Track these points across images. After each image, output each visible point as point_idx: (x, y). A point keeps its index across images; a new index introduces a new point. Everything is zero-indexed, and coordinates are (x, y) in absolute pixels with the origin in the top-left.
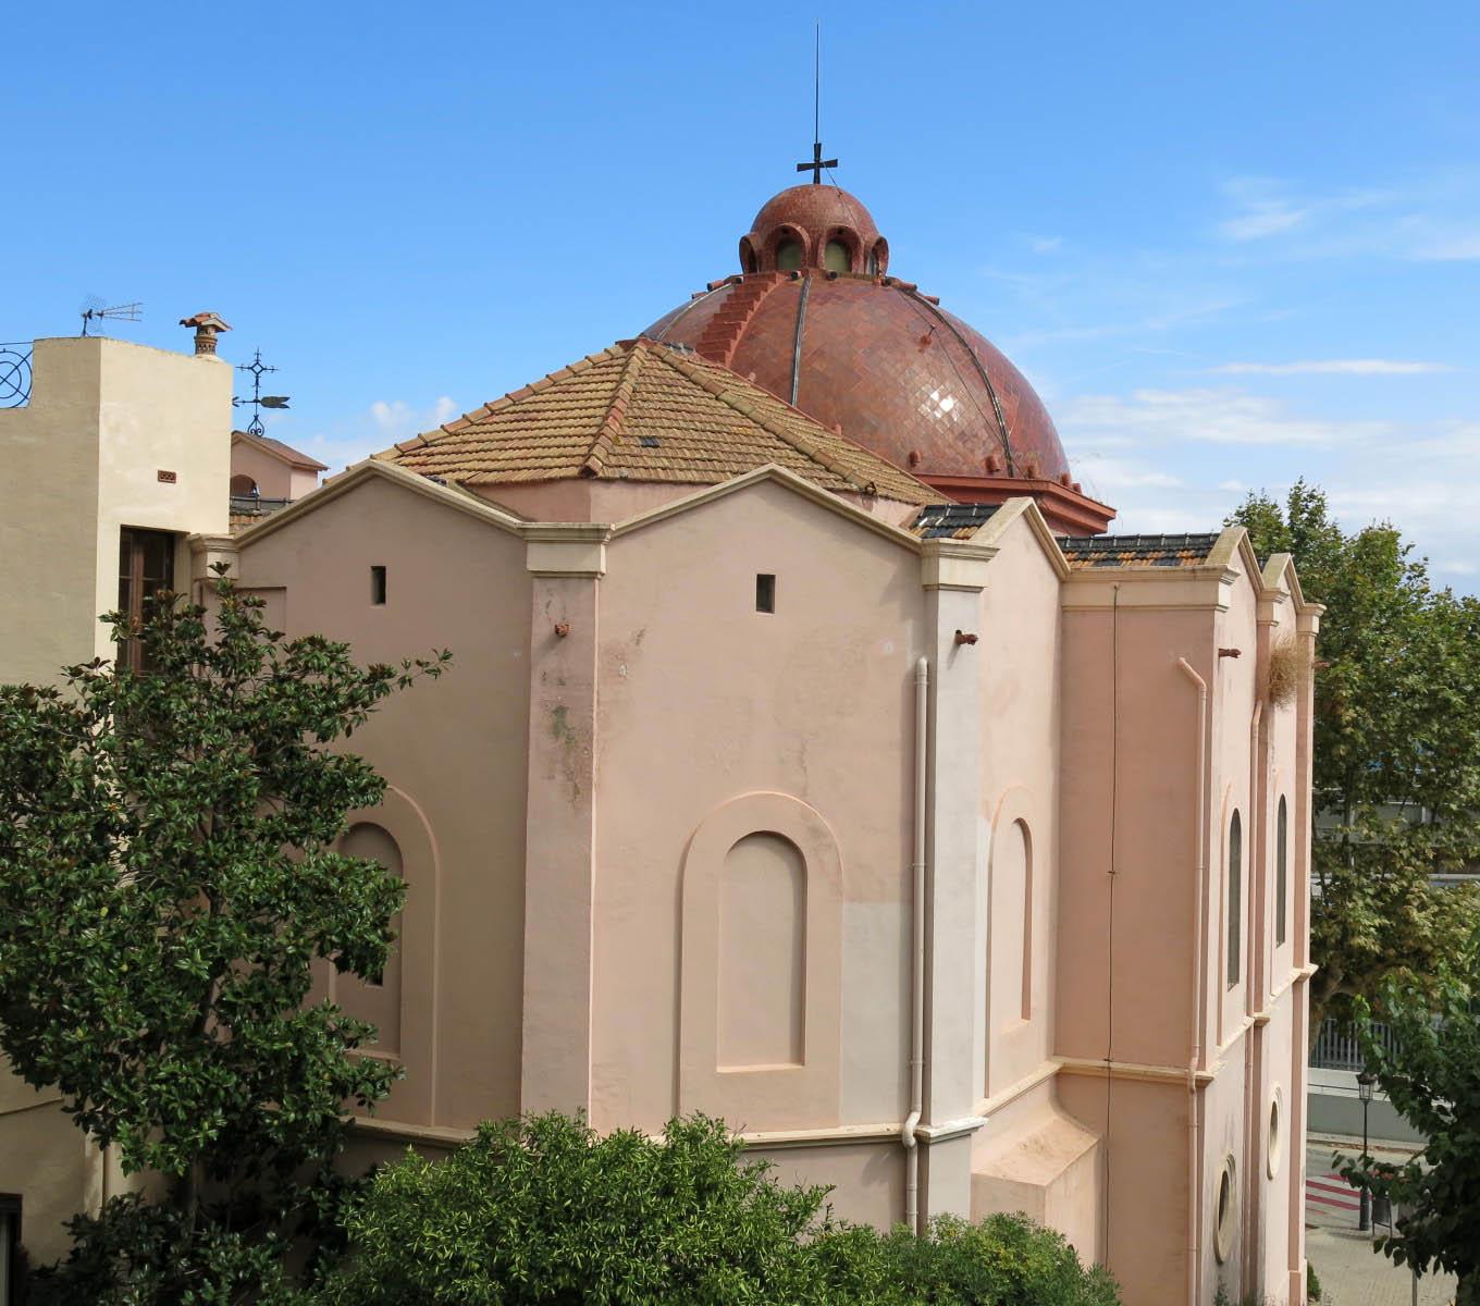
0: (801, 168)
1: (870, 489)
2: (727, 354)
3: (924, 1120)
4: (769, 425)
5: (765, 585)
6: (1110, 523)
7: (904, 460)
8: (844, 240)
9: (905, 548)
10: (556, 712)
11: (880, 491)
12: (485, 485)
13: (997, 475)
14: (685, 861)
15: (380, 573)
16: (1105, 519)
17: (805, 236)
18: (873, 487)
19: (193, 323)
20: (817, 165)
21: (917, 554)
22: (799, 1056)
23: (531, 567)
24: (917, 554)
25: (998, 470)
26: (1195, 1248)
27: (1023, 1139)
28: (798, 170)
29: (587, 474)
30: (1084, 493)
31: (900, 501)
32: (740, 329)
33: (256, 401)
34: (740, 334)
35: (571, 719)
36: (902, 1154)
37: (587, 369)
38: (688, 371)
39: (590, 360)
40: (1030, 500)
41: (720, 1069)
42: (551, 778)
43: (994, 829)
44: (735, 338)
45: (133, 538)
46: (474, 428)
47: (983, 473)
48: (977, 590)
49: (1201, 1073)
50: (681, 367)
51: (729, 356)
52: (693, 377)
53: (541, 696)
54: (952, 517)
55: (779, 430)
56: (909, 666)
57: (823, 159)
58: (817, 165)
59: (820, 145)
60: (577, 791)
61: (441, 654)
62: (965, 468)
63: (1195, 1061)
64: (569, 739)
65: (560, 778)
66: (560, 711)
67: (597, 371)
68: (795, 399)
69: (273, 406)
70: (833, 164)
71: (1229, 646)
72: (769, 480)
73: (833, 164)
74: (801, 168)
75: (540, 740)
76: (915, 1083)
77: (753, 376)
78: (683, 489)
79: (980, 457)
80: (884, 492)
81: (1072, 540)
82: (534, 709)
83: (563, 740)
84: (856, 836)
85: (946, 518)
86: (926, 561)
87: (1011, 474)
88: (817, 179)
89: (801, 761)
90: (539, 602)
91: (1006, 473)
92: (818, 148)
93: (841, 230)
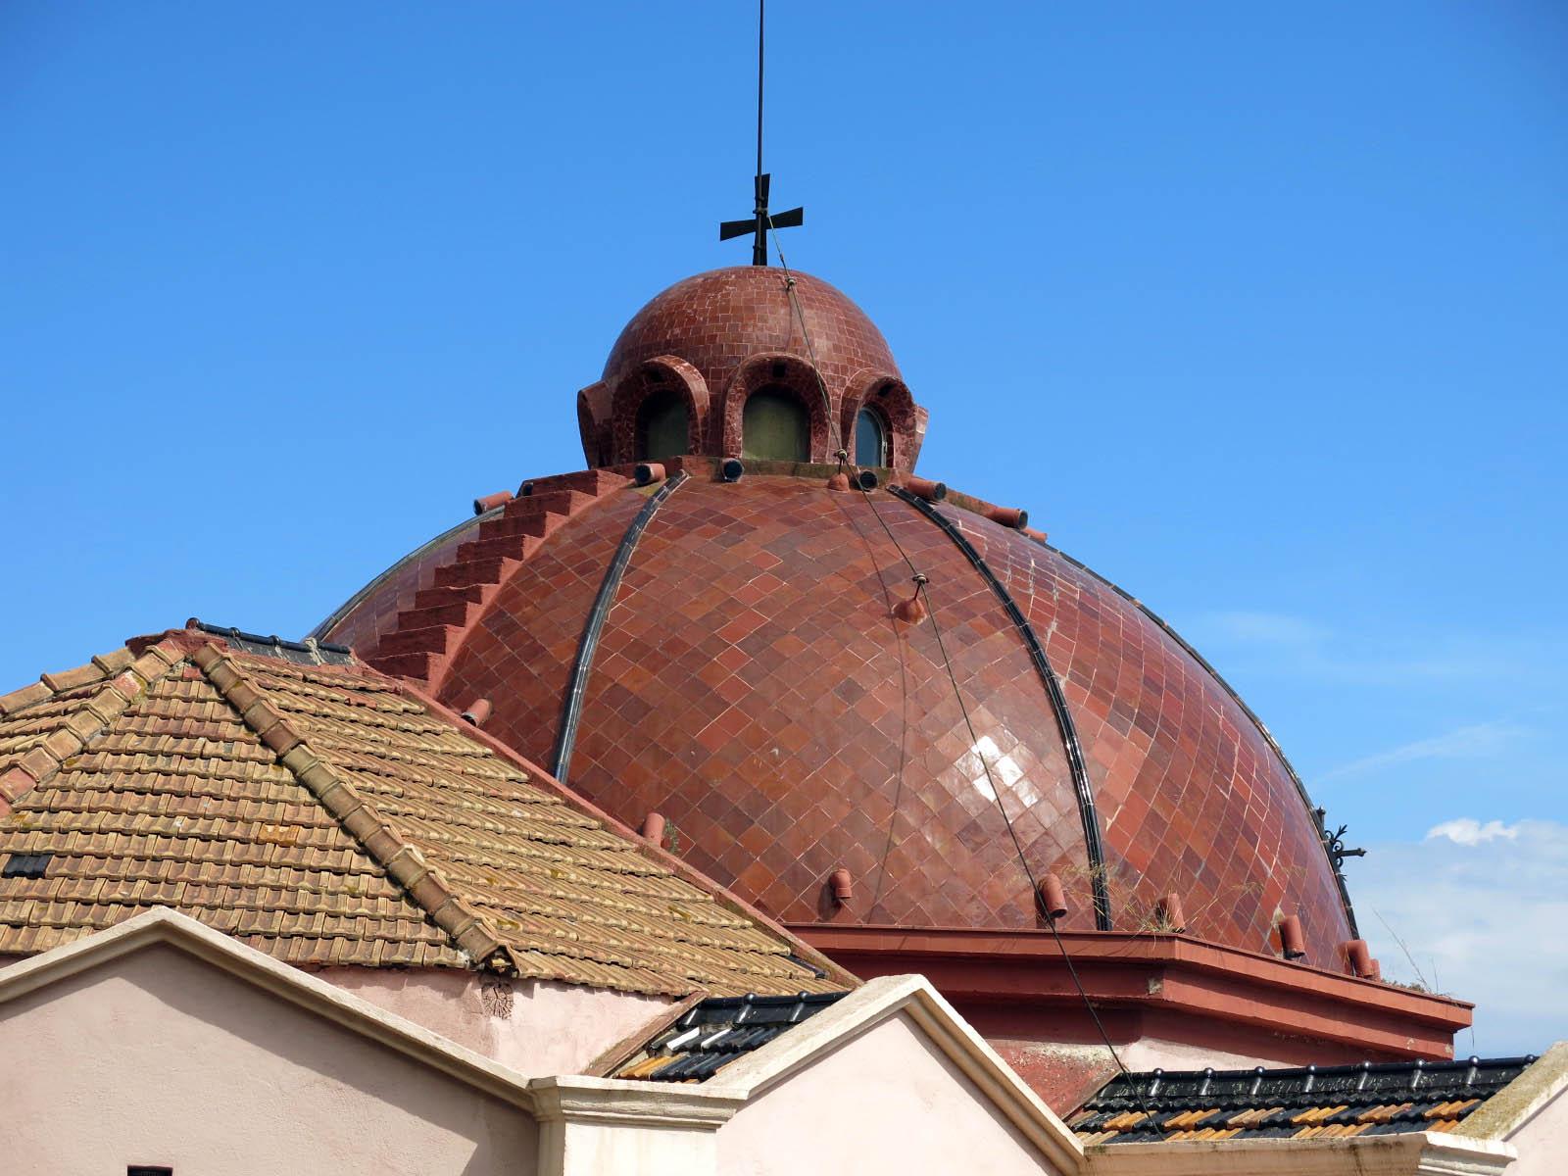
0: (730, 230)
1: (499, 962)
2: (434, 658)
4: (356, 820)
6: (1458, 1036)
7: (807, 896)
8: (786, 388)
9: (492, 1099)
11: (530, 964)
13: (1061, 925)
16: (1446, 1030)
17: (698, 386)
18: (508, 958)
20: (760, 225)
25: (1062, 913)
28: (723, 238)
30: (1387, 976)
31: (612, 989)
32: (479, 601)
34: (475, 613)
37: (36, 703)
38: (246, 700)
39: (48, 684)
40: (917, 982)
44: (461, 622)
47: (1027, 918)
50: (236, 693)
51: (440, 665)
52: (251, 714)
54: (748, 1025)
55: (367, 830)
57: (773, 210)
58: (760, 225)
59: (766, 178)
62: (973, 909)
67: (60, 706)
68: (565, 757)
70: (793, 218)
72: (161, 945)
73: (793, 218)
74: (730, 230)
77: (480, 709)
79: (1017, 883)
81: (1318, 1074)
85: (737, 1027)
86: (545, 1130)
87: (1103, 923)
88: (760, 256)
91: (1092, 920)
92: (763, 184)
93: (779, 367)
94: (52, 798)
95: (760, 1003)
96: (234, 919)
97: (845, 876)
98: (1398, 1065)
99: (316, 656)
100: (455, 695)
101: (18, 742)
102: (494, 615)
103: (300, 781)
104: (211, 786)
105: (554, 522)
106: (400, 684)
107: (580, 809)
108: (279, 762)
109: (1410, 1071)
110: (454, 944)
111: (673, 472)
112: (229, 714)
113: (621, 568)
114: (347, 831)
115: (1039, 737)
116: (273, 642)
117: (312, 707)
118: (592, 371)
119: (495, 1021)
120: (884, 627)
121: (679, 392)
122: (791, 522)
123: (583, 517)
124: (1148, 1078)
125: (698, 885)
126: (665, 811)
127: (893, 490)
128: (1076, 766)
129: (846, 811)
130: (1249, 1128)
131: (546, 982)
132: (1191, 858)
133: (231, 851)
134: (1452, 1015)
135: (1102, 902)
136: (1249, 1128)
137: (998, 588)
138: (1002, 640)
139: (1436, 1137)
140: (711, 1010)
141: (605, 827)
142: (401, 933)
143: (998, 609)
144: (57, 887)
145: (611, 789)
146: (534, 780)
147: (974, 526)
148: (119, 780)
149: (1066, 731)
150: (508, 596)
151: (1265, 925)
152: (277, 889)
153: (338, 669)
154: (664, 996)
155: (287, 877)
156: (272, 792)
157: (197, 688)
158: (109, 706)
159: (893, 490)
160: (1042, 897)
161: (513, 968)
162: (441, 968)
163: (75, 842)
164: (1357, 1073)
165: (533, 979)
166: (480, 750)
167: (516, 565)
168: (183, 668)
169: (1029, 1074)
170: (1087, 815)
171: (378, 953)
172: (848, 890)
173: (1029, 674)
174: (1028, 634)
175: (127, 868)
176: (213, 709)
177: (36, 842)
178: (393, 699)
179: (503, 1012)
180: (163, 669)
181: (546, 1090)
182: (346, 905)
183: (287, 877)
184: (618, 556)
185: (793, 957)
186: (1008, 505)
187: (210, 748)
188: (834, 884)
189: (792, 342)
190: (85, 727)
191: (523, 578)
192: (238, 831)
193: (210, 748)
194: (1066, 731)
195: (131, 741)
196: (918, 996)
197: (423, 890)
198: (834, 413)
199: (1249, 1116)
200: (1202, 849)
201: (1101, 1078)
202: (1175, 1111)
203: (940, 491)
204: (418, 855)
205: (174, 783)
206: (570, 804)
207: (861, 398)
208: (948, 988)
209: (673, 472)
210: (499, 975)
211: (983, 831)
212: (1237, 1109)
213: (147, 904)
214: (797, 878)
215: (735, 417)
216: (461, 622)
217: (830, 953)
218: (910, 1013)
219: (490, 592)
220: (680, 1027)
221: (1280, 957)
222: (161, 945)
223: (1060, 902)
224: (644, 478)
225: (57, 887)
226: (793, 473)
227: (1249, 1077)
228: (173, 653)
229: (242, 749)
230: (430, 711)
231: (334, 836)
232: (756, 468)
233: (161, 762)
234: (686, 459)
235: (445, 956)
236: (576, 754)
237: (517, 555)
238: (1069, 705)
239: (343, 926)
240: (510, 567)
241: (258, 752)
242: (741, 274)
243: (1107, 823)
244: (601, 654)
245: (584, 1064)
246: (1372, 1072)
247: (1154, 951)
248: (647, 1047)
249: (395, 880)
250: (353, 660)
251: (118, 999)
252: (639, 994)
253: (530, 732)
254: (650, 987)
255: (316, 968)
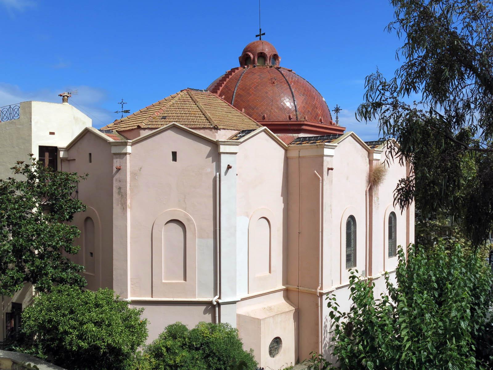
1: (216, 127)
3: (220, 298)
4: (203, 111)
5: (174, 154)
7: (261, 118)
8: (262, 56)
10: (119, 189)
12: (124, 131)
13: (292, 120)
14: (390, 237)
15: (90, 154)
17: (252, 56)
19: (61, 96)
21: (216, 144)
22: (185, 279)
23: (112, 152)
24: (216, 144)
26: (320, 341)
27: (266, 306)
29: (139, 127)
33: (122, 112)
34: (223, 85)
35: (122, 191)
36: (212, 308)
41: (163, 281)
42: (118, 205)
43: (250, 220)
45: (43, 149)
46: (135, 116)
47: (288, 119)
48: (236, 153)
49: (321, 291)
50: (192, 96)
51: (219, 92)
53: (115, 184)
56: (215, 175)
60: (124, 209)
61: (86, 174)
63: (319, 287)
64: (122, 196)
65: (120, 205)
66: (120, 188)
68: (233, 102)
69: (126, 113)
70: (264, 34)
71: (330, 167)
72: (174, 126)
73: (264, 34)
74: (257, 36)
75: (115, 196)
76: (217, 289)
77: (223, 97)
78: (147, 130)
80: (222, 127)
82: (114, 188)
83: (120, 196)
84: (199, 222)
89: (185, 201)
90: (115, 161)
92: (260, 30)
93: (261, 53)
94: (168, 110)
95: (248, 130)
96: (183, 123)
97: (265, 115)
98: (335, 135)
99: (204, 91)
100: (220, 95)
101: (164, 104)
102: (225, 85)
103: (197, 107)
104: (187, 107)
105: (233, 74)
106: (214, 94)
107: (234, 108)
108: (195, 104)
109: (330, 136)
110: (211, 125)
111: (248, 67)
112: (191, 99)
113: (240, 79)
114: (202, 112)
115: (290, 98)
116: (198, 90)
117: (201, 97)
118: (240, 54)
119: (216, 134)
120: (271, 85)
121: (249, 57)
122: (261, 72)
123: (237, 73)
124: (301, 138)
125: (247, 117)
126: (244, 108)
127: (275, 68)
128: (294, 101)
129: (266, 107)
130: (311, 143)
131: (222, 129)
132: (309, 111)
133: (188, 115)
134: (343, 129)
135: (297, 117)
136: (311, 143)
137: (286, 79)
138: (286, 86)
139: (375, 149)
140: (243, 132)
141: (236, 110)
142: (205, 124)
143: (286, 82)
144: (167, 120)
145: (238, 106)
146: (229, 105)
147: (284, 72)
148: (176, 107)
149: (293, 96)
150: (227, 83)
151: (318, 119)
152: (192, 119)
153: (206, 93)
154: (237, 130)
155: (194, 118)
156: (194, 108)
157: (188, 96)
158: (176, 99)
159: (275, 68)
160: (289, 117)
161: (218, 127)
162: (209, 128)
163: (170, 115)
164: (324, 136)
165: (220, 129)
166: (222, 102)
167: (228, 79)
168: (186, 94)
169: (278, 136)
170: (295, 107)
171: (202, 126)
172: (266, 117)
173: (289, 90)
174: (289, 85)
175: (175, 117)
176: (189, 98)
177: (166, 115)
178: (213, 96)
179: (217, 133)
180: (184, 94)
181: (218, 141)
182: (200, 121)
183: (194, 118)
184: (240, 77)
185: (257, 125)
186: (290, 69)
187: (188, 103)
188: (264, 116)
189: (262, 50)
190: (173, 101)
191: (229, 81)
192: (189, 113)
193: (188, 103)
194: (293, 96)
195: (179, 103)
196: (265, 129)
197: (209, 119)
198: (268, 58)
199: (312, 142)
200: (310, 110)
201: (295, 138)
202: (303, 141)
203: (280, 68)
204: (209, 115)
205: (183, 107)
206: (232, 108)
207: (272, 56)
208: (271, 128)
209: (248, 67)
210: (216, 128)
211: (283, 109)
212: (310, 141)
213: (172, 122)
214: (260, 115)
215: (256, 60)
216: (221, 86)
217: (261, 124)
218: (265, 131)
219: (225, 83)
220: (239, 133)
221: (320, 123)
222: (174, 126)
223: (292, 117)
224: (244, 68)
225: (167, 120)
226: (263, 66)
227: (312, 137)
228: (185, 92)
229: (192, 103)
230: (217, 97)
231: (200, 113)
232: (258, 66)
233: (182, 105)
234: (249, 65)
235: (210, 126)
236: (234, 102)
237: (228, 78)
238: (294, 93)
239: (199, 123)
240: (227, 79)
241: (193, 103)
242: (257, 42)
243: (298, 107)
244: (237, 89)
245: (227, 138)
246: (326, 136)
247: (302, 123)
248: (235, 136)
249: (206, 118)
250: (208, 92)
251: (170, 133)
252: (234, 130)
253: (229, 100)
254: (236, 129)
255: (190, 128)
